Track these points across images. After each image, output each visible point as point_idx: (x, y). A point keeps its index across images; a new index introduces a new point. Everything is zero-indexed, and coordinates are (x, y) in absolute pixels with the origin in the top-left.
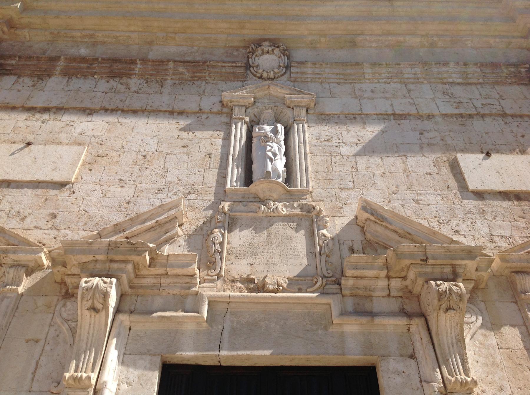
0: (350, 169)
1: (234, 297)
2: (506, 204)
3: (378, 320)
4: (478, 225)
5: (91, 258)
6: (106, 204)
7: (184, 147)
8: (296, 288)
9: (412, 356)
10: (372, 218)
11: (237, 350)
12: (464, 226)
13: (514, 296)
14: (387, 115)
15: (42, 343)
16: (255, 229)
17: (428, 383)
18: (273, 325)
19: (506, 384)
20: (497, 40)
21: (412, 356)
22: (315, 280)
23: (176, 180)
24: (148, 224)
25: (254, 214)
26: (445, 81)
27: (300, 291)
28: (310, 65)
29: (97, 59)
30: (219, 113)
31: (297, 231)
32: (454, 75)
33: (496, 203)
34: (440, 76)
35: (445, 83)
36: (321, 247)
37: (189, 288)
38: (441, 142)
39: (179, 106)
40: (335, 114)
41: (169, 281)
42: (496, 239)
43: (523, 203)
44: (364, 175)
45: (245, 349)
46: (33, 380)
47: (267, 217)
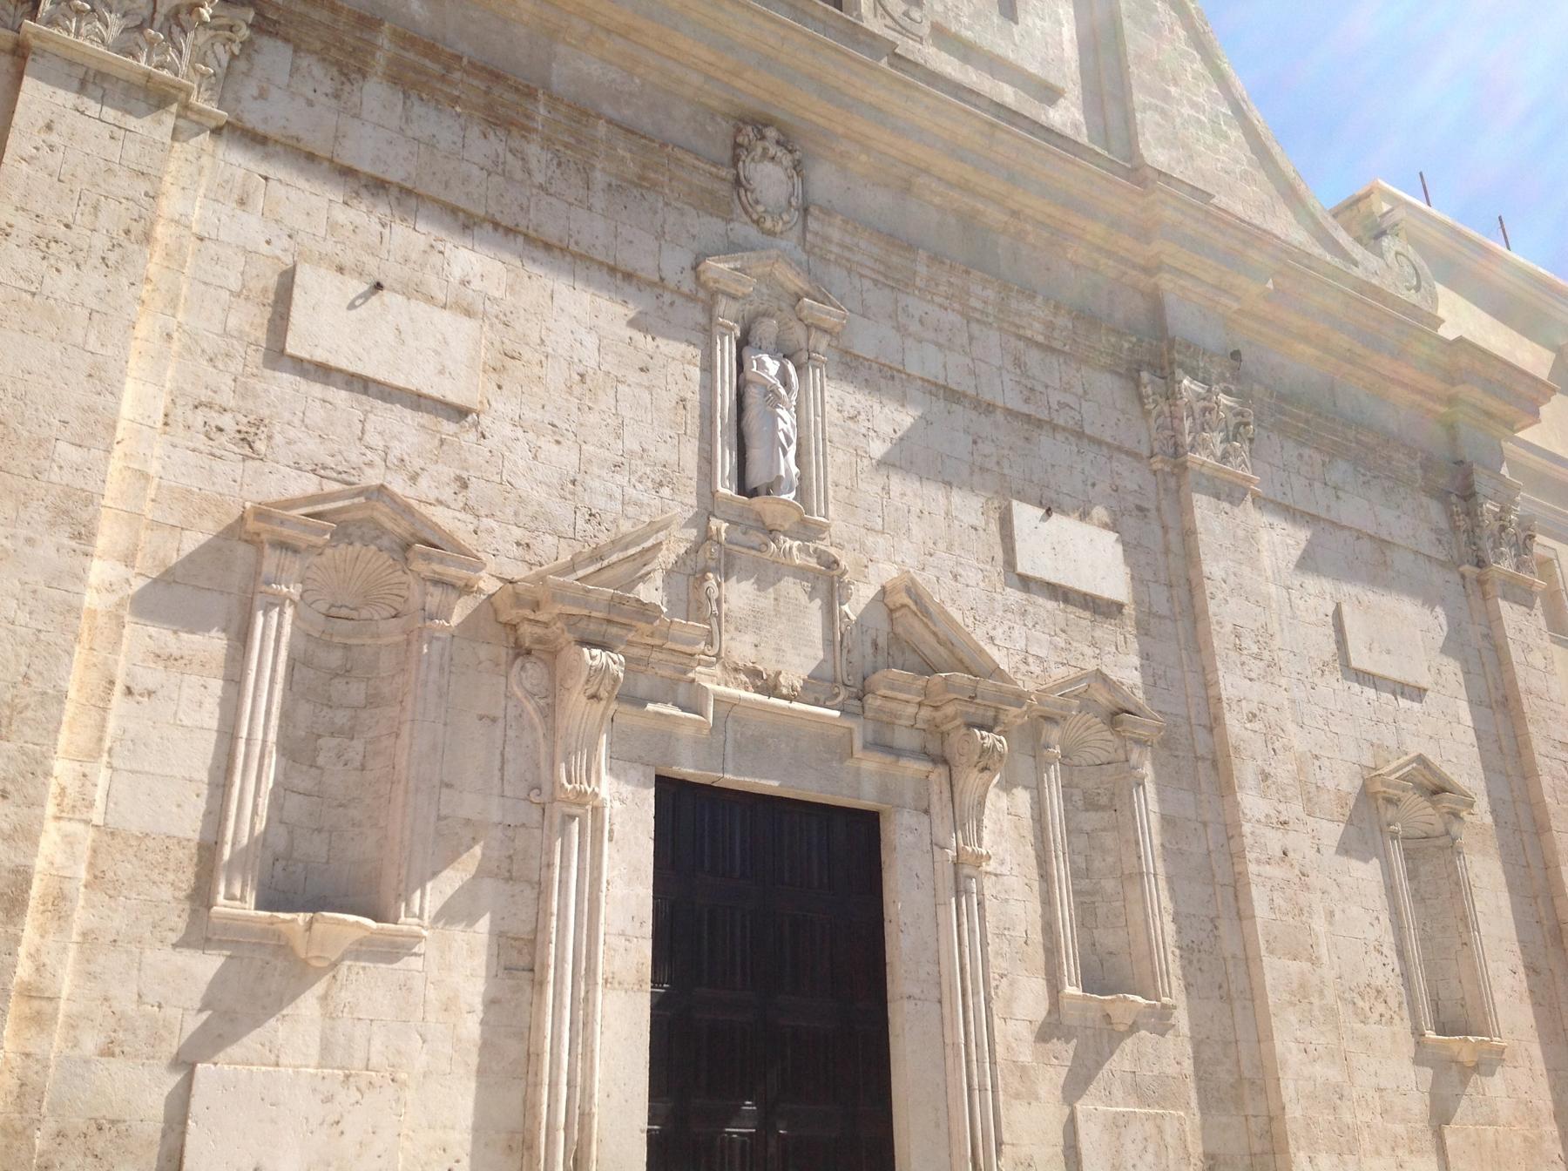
0: (880, 491)
1: (745, 700)
2: (1051, 605)
3: (904, 762)
4: (1016, 634)
5: (586, 612)
6: (539, 477)
7: (642, 370)
8: (811, 697)
9: (927, 812)
10: (913, 607)
11: (744, 775)
12: (1000, 631)
13: (1033, 748)
14: (936, 385)
15: (501, 723)
16: (758, 581)
17: (942, 848)
18: (783, 746)
19: (1008, 858)
20: (1111, 263)
21: (927, 812)
22: (836, 690)
23: (637, 448)
24: (632, 551)
25: (758, 554)
26: (1021, 332)
27: (816, 703)
28: (838, 221)
29: (460, 58)
30: (691, 298)
31: (811, 599)
32: (1037, 325)
33: (1041, 601)
34: (1017, 321)
35: (1020, 337)
36: (842, 635)
37: (685, 673)
38: (996, 468)
39: (628, 258)
40: (864, 358)
41: (661, 656)
42: (1031, 660)
43: (1070, 608)
44: (897, 510)
45: (753, 775)
46: (502, 779)
47: (773, 562)
